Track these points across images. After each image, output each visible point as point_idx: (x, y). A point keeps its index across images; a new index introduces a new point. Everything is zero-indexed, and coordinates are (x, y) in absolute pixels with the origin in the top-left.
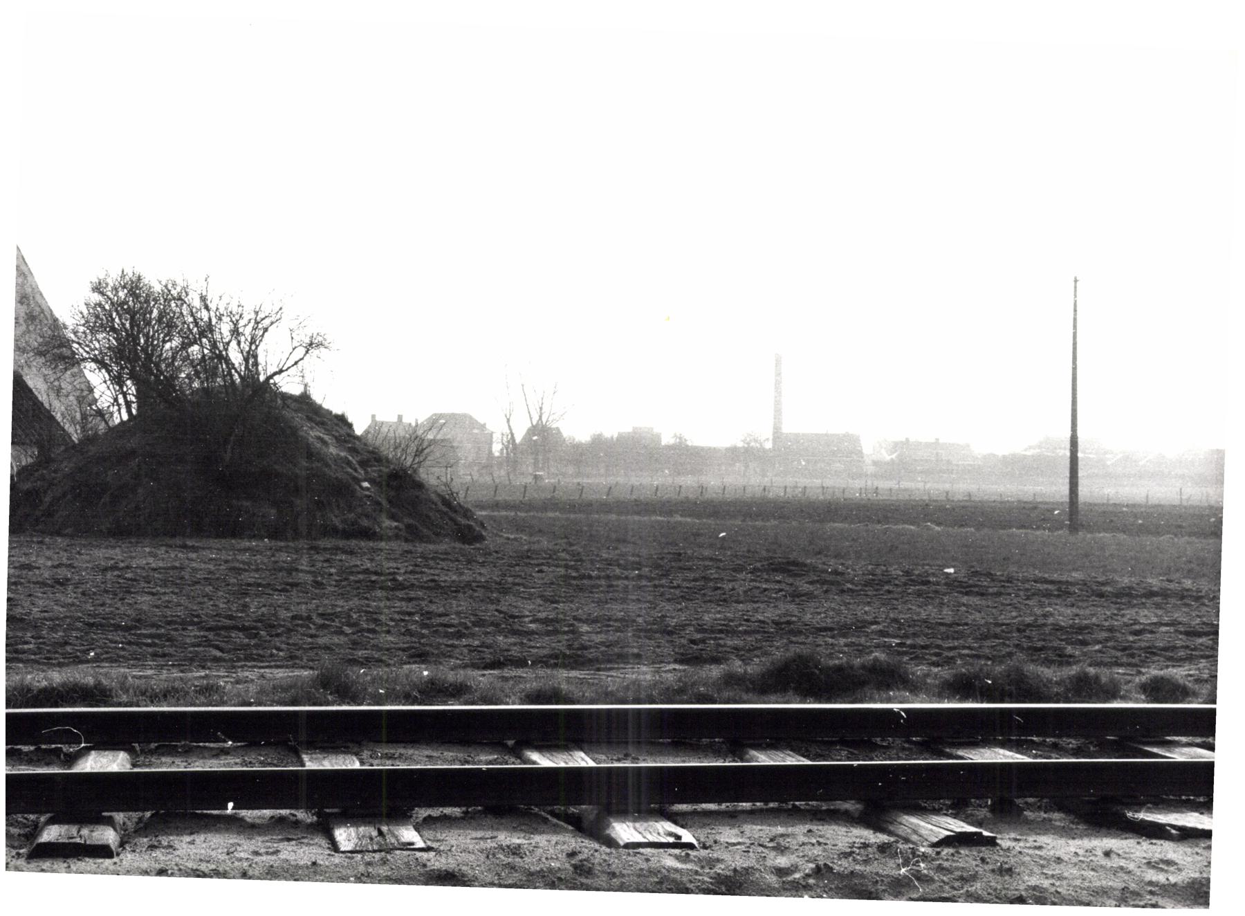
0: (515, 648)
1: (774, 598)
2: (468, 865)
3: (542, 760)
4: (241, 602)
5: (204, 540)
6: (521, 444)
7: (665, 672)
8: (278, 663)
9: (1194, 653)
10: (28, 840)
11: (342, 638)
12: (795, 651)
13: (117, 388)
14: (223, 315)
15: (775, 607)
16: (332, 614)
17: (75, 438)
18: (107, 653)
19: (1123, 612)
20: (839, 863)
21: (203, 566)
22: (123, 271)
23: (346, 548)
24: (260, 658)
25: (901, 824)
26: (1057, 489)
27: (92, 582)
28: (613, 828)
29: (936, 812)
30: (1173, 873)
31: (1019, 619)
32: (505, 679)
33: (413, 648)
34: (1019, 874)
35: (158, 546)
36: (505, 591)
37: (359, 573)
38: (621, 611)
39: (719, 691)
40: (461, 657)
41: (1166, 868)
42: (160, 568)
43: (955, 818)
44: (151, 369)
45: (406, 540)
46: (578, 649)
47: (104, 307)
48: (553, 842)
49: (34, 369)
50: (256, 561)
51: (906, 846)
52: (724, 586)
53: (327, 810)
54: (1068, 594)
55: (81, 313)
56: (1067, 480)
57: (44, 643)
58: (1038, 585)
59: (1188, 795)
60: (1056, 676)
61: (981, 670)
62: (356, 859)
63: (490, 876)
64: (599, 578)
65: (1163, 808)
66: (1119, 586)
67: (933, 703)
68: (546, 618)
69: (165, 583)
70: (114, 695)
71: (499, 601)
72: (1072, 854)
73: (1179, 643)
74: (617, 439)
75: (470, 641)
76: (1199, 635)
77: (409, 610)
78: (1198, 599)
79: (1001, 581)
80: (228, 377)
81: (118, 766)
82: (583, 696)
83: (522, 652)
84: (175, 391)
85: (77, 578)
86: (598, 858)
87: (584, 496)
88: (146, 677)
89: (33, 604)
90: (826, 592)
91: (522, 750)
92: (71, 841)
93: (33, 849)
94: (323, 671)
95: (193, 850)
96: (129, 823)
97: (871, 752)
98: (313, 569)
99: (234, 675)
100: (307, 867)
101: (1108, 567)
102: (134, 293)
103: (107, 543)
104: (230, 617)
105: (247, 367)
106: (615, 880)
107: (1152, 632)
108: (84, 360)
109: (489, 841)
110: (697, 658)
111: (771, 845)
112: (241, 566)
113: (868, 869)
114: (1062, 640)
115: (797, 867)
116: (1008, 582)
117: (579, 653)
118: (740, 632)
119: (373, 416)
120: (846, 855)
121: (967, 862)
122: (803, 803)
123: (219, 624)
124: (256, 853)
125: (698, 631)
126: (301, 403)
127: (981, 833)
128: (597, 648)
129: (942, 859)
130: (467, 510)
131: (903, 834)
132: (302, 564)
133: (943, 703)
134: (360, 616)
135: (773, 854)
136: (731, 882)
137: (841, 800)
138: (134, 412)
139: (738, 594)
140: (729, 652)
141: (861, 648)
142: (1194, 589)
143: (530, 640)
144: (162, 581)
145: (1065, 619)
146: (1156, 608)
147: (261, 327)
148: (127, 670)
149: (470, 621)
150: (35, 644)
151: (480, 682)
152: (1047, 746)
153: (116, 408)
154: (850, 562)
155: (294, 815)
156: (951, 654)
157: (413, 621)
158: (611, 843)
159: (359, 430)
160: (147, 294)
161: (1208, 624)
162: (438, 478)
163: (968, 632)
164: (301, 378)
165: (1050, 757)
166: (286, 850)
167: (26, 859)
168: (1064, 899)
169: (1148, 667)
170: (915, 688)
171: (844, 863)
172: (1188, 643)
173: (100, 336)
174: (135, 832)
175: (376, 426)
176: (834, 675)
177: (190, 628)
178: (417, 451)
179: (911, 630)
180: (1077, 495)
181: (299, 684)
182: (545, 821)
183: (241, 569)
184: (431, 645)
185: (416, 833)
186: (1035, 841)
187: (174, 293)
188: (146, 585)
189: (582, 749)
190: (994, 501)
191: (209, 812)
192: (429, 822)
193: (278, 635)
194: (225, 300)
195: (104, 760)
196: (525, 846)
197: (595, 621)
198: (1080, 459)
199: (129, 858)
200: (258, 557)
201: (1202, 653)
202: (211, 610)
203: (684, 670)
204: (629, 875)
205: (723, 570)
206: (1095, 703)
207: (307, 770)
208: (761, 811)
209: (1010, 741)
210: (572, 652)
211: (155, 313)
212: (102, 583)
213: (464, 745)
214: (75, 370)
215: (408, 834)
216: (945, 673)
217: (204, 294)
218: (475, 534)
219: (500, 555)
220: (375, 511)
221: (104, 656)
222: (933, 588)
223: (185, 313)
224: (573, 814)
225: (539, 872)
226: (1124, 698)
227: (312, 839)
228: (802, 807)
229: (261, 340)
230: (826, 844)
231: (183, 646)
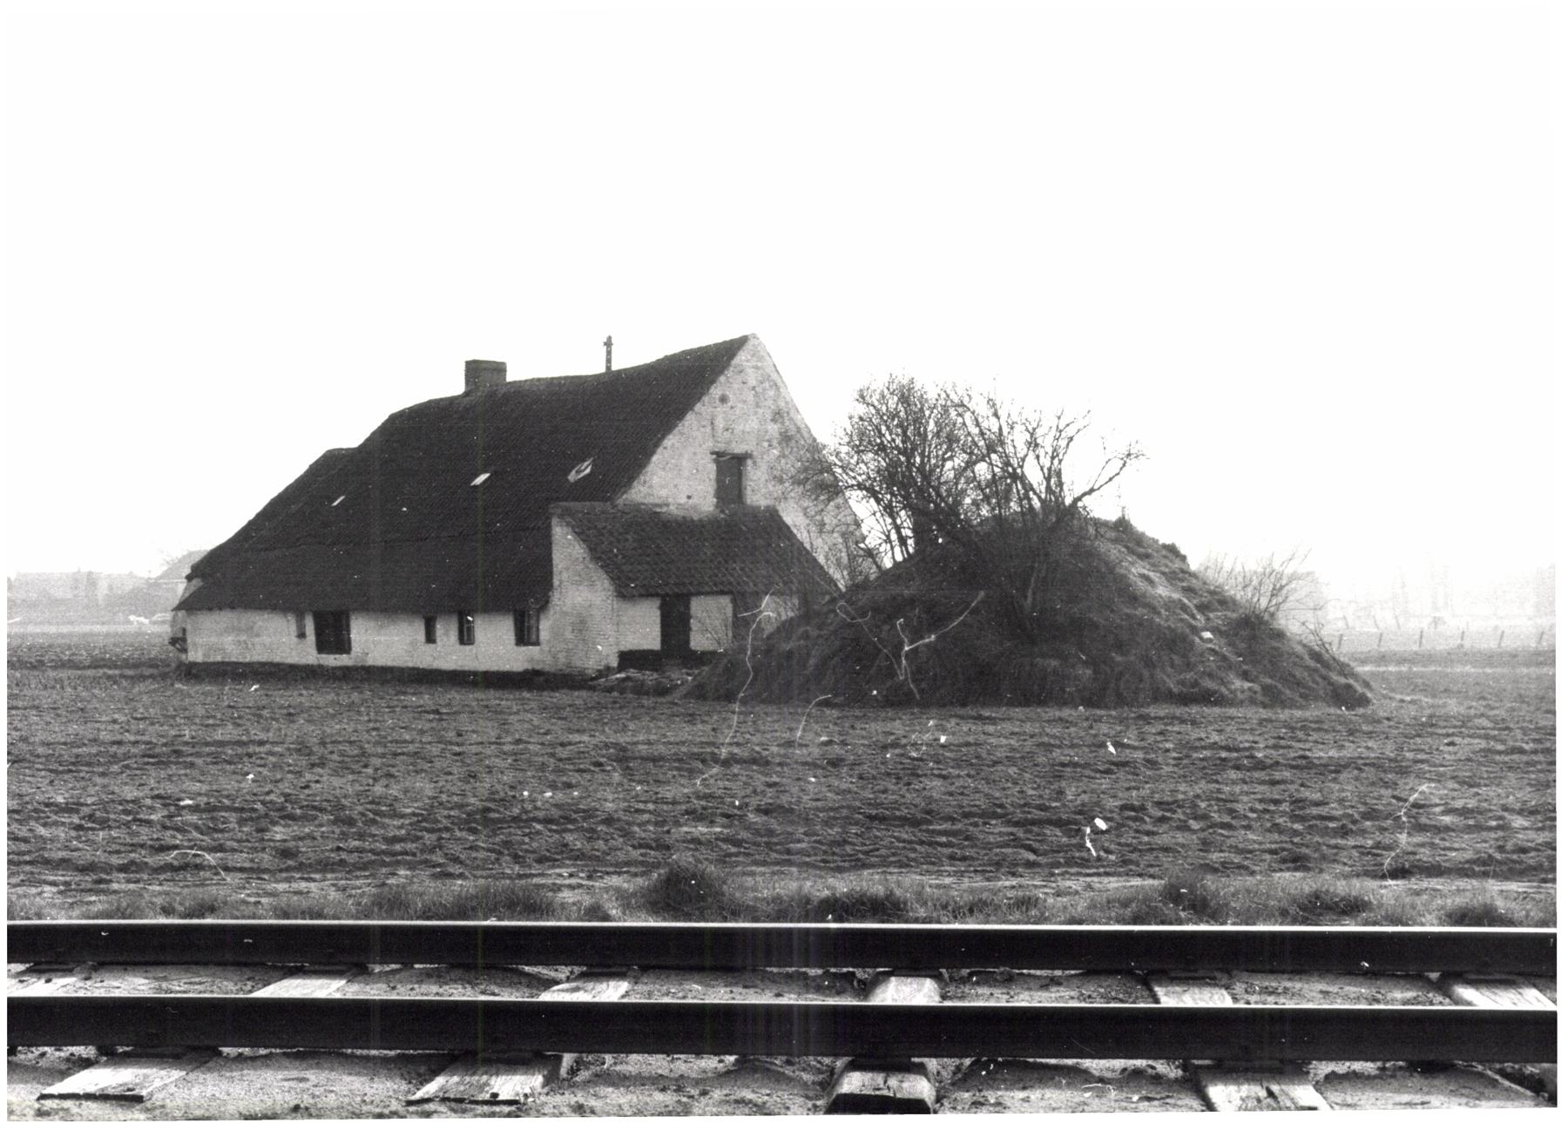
0: (1422, 850)
4: (1055, 786)
8: (1108, 870)
16: (1173, 803)
17: (841, 585)
18: (894, 854)
21: (1004, 742)
33: (1284, 849)
36: (1403, 772)
37: (1204, 748)
45: (1265, 707)
46: (1513, 852)
50: (1070, 734)
53: (1196, 1062)
64: (1535, 752)
68: (1464, 808)
69: (959, 763)
71: (1396, 784)
75: (1359, 841)
85: (852, 757)
89: (803, 790)
92: (878, 1093)
96: (944, 1073)
99: (1054, 885)
103: (883, 715)
105: (1048, 488)
123: (1029, 816)
128: (1539, 850)
134: (1210, 805)
147: (1065, 436)
149: (1360, 813)
150: (809, 842)
155: (1153, 1068)
174: (953, 1084)
177: (994, 822)
178: (1274, 589)
182: (1494, 1083)
188: (935, 766)
189: (1535, 986)
191: (1043, 1060)
192: (1332, 1078)
197: (1533, 812)
211: (931, 426)
213: (1370, 978)
214: (840, 500)
219: (1392, 723)
221: (892, 859)
224: (1532, 1075)
231: (988, 846)
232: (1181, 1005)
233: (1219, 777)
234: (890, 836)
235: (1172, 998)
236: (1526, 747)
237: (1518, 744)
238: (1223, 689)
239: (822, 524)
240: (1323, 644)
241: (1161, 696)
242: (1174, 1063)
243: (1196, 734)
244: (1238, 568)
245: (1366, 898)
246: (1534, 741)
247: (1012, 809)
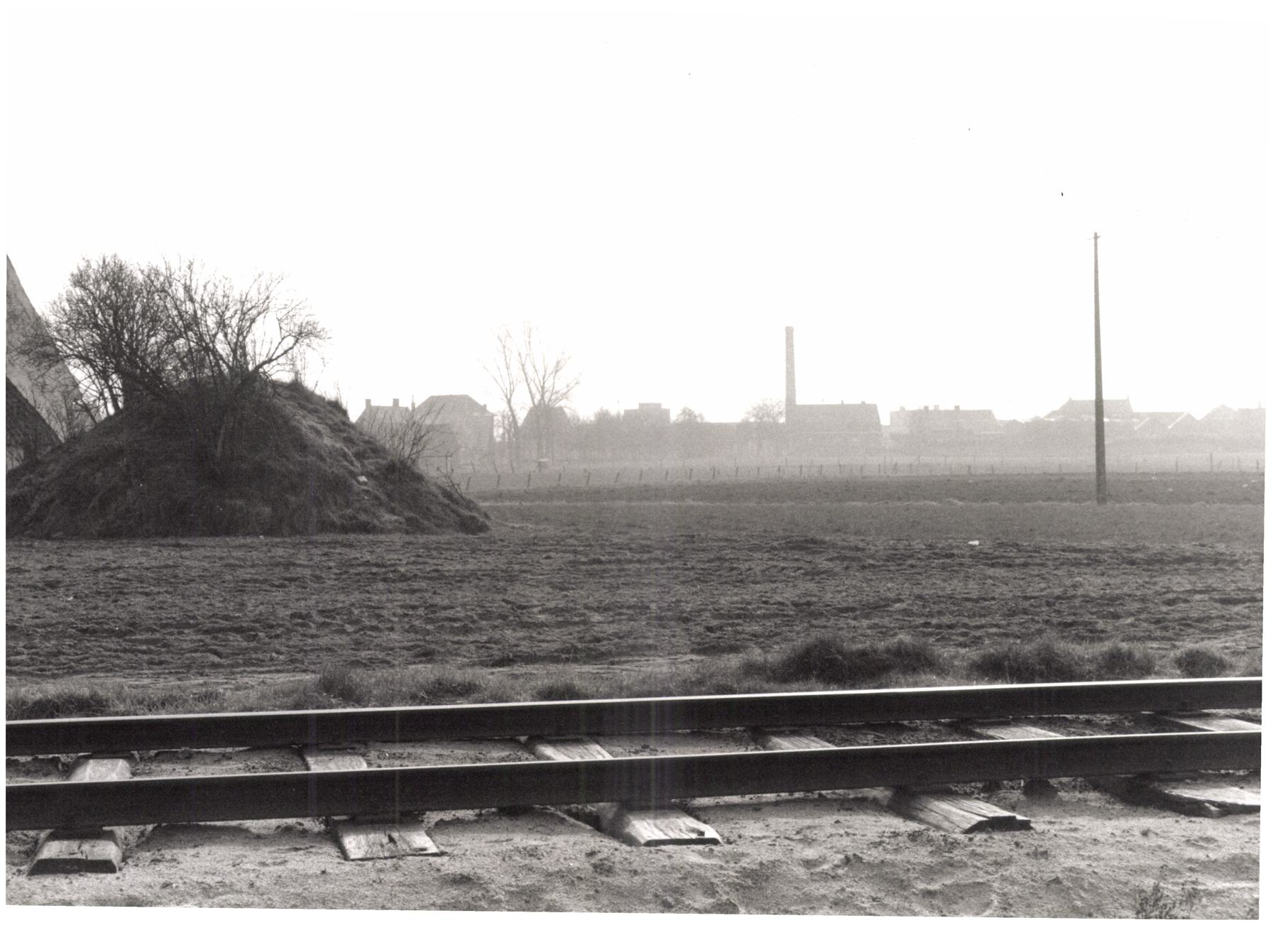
0: (524, 643)
1: (793, 577)
2: (483, 868)
3: (556, 755)
5: (198, 539)
6: (524, 426)
7: (682, 663)
8: (279, 668)
9: (1229, 623)
10: (28, 857)
11: (344, 637)
12: (816, 636)
13: (103, 382)
14: (208, 307)
15: (794, 586)
17: (61, 436)
18: (102, 662)
19: (1155, 579)
20: (869, 853)
21: (197, 563)
22: (104, 262)
23: (345, 542)
24: (260, 663)
25: (932, 811)
26: (1084, 460)
27: (84, 583)
28: (633, 826)
29: (968, 795)
30: (1213, 850)
31: (1048, 590)
32: (515, 677)
34: (1055, 857)
36: (512, 579)
37: (359, 565)
38: (633, 597)
39: (738, 681)
40: (468, 655)
41: (1206, 845)
42: (153, 567)
43: (987, 802)
44: (136, 363)
45: (407, 533)
46: (590, 642)
47: (86, 303)
48: (571, 843)
49: (18, 367)
51: (938, 834)
52: (740, 566)
53: (336, 818)
54: (1099, 562)
55: (64, 310)
56: (1094, 449)
57: (37, 653)
58: (1066, 554)
59: (1227, 769)
60: (1088, 654)
61: (1010, 649)
62: (367, 866)
63: (507, 878)
65: (1202, 784)
66: (1151, 552)
67: (961, 685)
68: (556, 607)
69: (158, 581)
70: (110, 704)
71: (506, 590)
72: (1109, 835)
73: (1214, 613)
74: (624, 417)
76: (1236, 602)
77: (412, 603)
78: (1232, 563)
79: (1028, 552)
80: (216, 368)
81: (117, 775)
82: (597, 691)
83: (532, 647)
84: (162, 383)
85: (68, 580)
86: (618, 857)
87: (591, 483)
88: (143, 686)
89: (24, 610)
90: (847, 568)
91: (535, 745)
93: (34, 866)
94: (326, 674)
95: (197, 863)
96: (130, 838)
97: (898, 735)
98: (311, 563)
99: (234, 682)
100: (317, 876)
101: (1139, 535)
102: (117, 285)
103: (97, 545)
104: (226, 618)
105: (235, 357)
106: (637, 878)
107: (1186, 601)
108: (68, 356)
109: (504, 843)
110: (714, 647)
111: (798, 837)
112: (237, 562)
113: (899, 857)
114: (1092, 614)
115: (825, 859)
116: (1035, 552)
117: (591, 645)
118: (758, 616)
119: (368, 402)
120: (876, 845)
121: (1000, 847)
122: (830, 791)
123: (216, 625)
124: (264, 864)
125: (715, 617)
126: (293, 391)
127: (1014, 817)
128: (610, 640)
129: (975, 845)
130: (470, 502)
131: (935, 822)
132: (300, 559)
133: (972, 685)
135: (800, 846)
136: (757, 875)
137: (868, 787)
138: (120, 405)
139: (755, 573)
140: (748, 640)
141: (884, 630)
142: (1228, 553)
143: (539, 633)
144: (155, 579)
145: (1095, 590)
146: (1190, 574)
147: (248, 318)
148: (123, 680)
149: (477, 614)
150: (28, 654)
151: (489, 680)
152: (1080, 723)
153: (102, 402)
154: (871, 538)
155: (301, 824)
156: (978, 633)
157: (417, 615)
158: (631, 841)
159: (354, 416)
160: (129, 287)
161: (1244, 590)
162: (438, 469)
163: (996, 607)
164: (291, 367)
165: (1084, 734)
166: (294, 860)
167: (28, 875)
168: (1102, 879)
169: (1183, 640)
170: (942, 670)
171: (874, 852)
172: (1224, 613)
173: (83, 333)
174: (137, 846)
175: (371, 411)
176: (857, 661)
177: (186, 631)
179: (936, 608)
180: (1104, 465)
181: (301, 688)
182: (562, 821)
184: (437, 643)
185: (428, 839)
186: (1070, 823)
187: (157, 284)
188: (139, 585)
189: (598, 743)
190: (1018, 474)
191: (212, 823)
192: (441, 824)
193: (277, 636)
195: (103, 769)
196: (542, 848)
198: (1106, 425)
199: (132, 872)
200: (254, 553)
201: (1238, 623)
202: (207, 610)
203: (702, 661)
204: (651, 872)
205: (739, 550)
206: (1129, 679)
207: (312, 774)
208: (787, 802)
209: (1041, 719)
210: (583, 645)
211: (139, 307)
212: (94, 584)
213: (475, 743)
214: (59, 366)
215: (420, 840)
216: (973, 654)
219: (505, 543)
220: (373, 506)
221: (99, 665)
222: (958, 560)
223: (169, 306)
224: (591, 813)
225: (558, 872)
226: (1158, 674)
227: (320, 848)
228: (829, 797)
229: (248, 332)
230: (854, 835)
231: (181, 652)
232: (327, 771)
233: (369, 588)
234: (98, 646)
235: (320, 765)
236: (603, 558)
237: (597, 556)
238: (375, 521)
239: (44, 386)
240: (453, 485)
241: (326, 526)
242: (318, 820)
243: (354, 554)
244: (387, 421)
245: (477, 683)
246: (609, 553)
247: (202, 620)
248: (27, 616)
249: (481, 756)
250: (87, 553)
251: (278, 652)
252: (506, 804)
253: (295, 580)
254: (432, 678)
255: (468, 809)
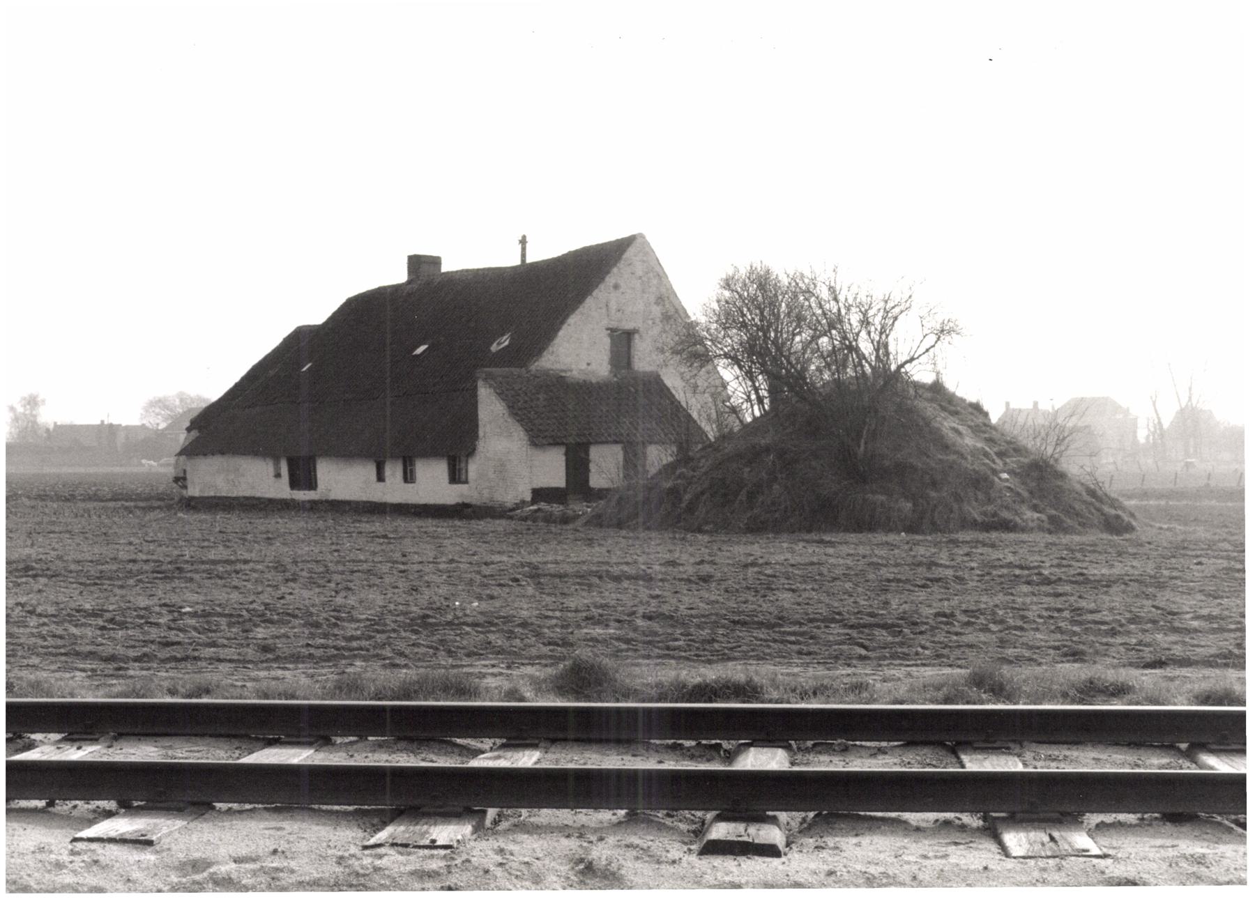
0: (1175, 647)
10: (697, 836)
17: (711, 436)
21: (841, 561)
24: (905, 656)
32: (1172, 679)
33: (1065, 646)
35: (796, 542)
36: (1161, 586)
37: (1001, 567)
45: (1050, 532)
53: (994, 815)
57: (693, 640)
68: (1209, 615)
69: (805, 579)
91: (1197, 754)
92: (740, 839)
95: (858, 852)
96: (793, 824)
99: (881, 673)
103: (744, 539)
104: (872, 615)
105: (877, 357)
112: (880, 561)
119: (1007, 404)
124: (925, 857)
138: (767, 407)
147: (891, 317)
149: (1125, 618)
151: (1143, 682)
155: (959, 819)
159: (994, 419)
162: (1082, 467)
174: (800, 832)
175: (1010, 414)
177: (833, 625)
182: (1230, 830)
183: (879, 564)
188: (786, 582)
192: (1101, 826)
193: (921, 633)
194: (854, 290)
214: (710, 367)
215: (1080, 840)
217: (833, 284)
218: (1124, 524)
229: (891, 330)
231: (829, 644)
235: (975, 764)
238: (1017, 519)
239: (696, 387)
243: (995, 554)
244: (1030, 422)
248: (682, 607)
249: (1140, 762)
250: (736, 547)
251: (924, 647)
252: (1169, 810)
253: (938, 580)
254: (1083, 677)
255: (1129, 812)
